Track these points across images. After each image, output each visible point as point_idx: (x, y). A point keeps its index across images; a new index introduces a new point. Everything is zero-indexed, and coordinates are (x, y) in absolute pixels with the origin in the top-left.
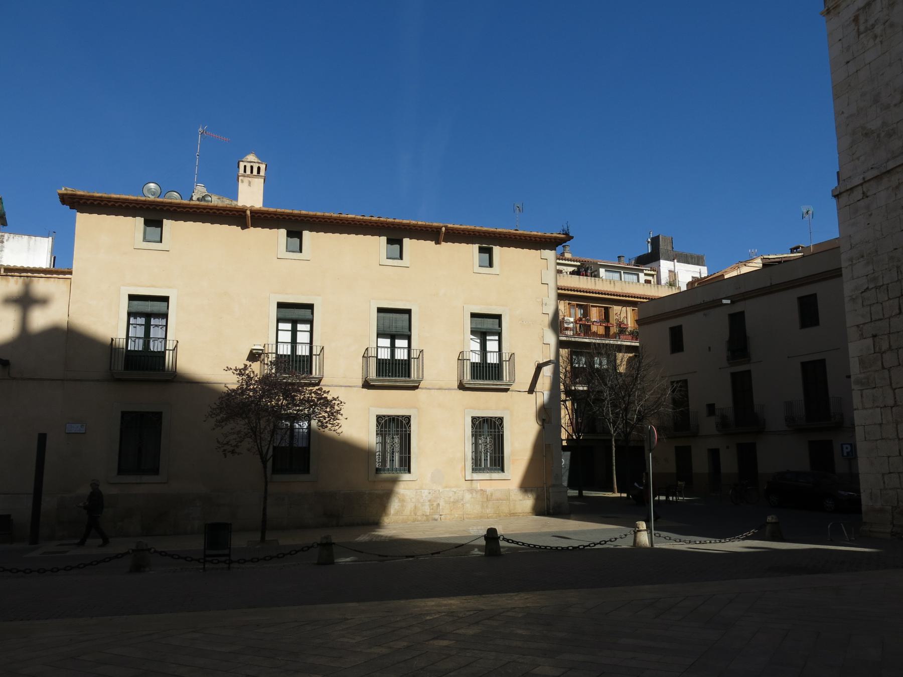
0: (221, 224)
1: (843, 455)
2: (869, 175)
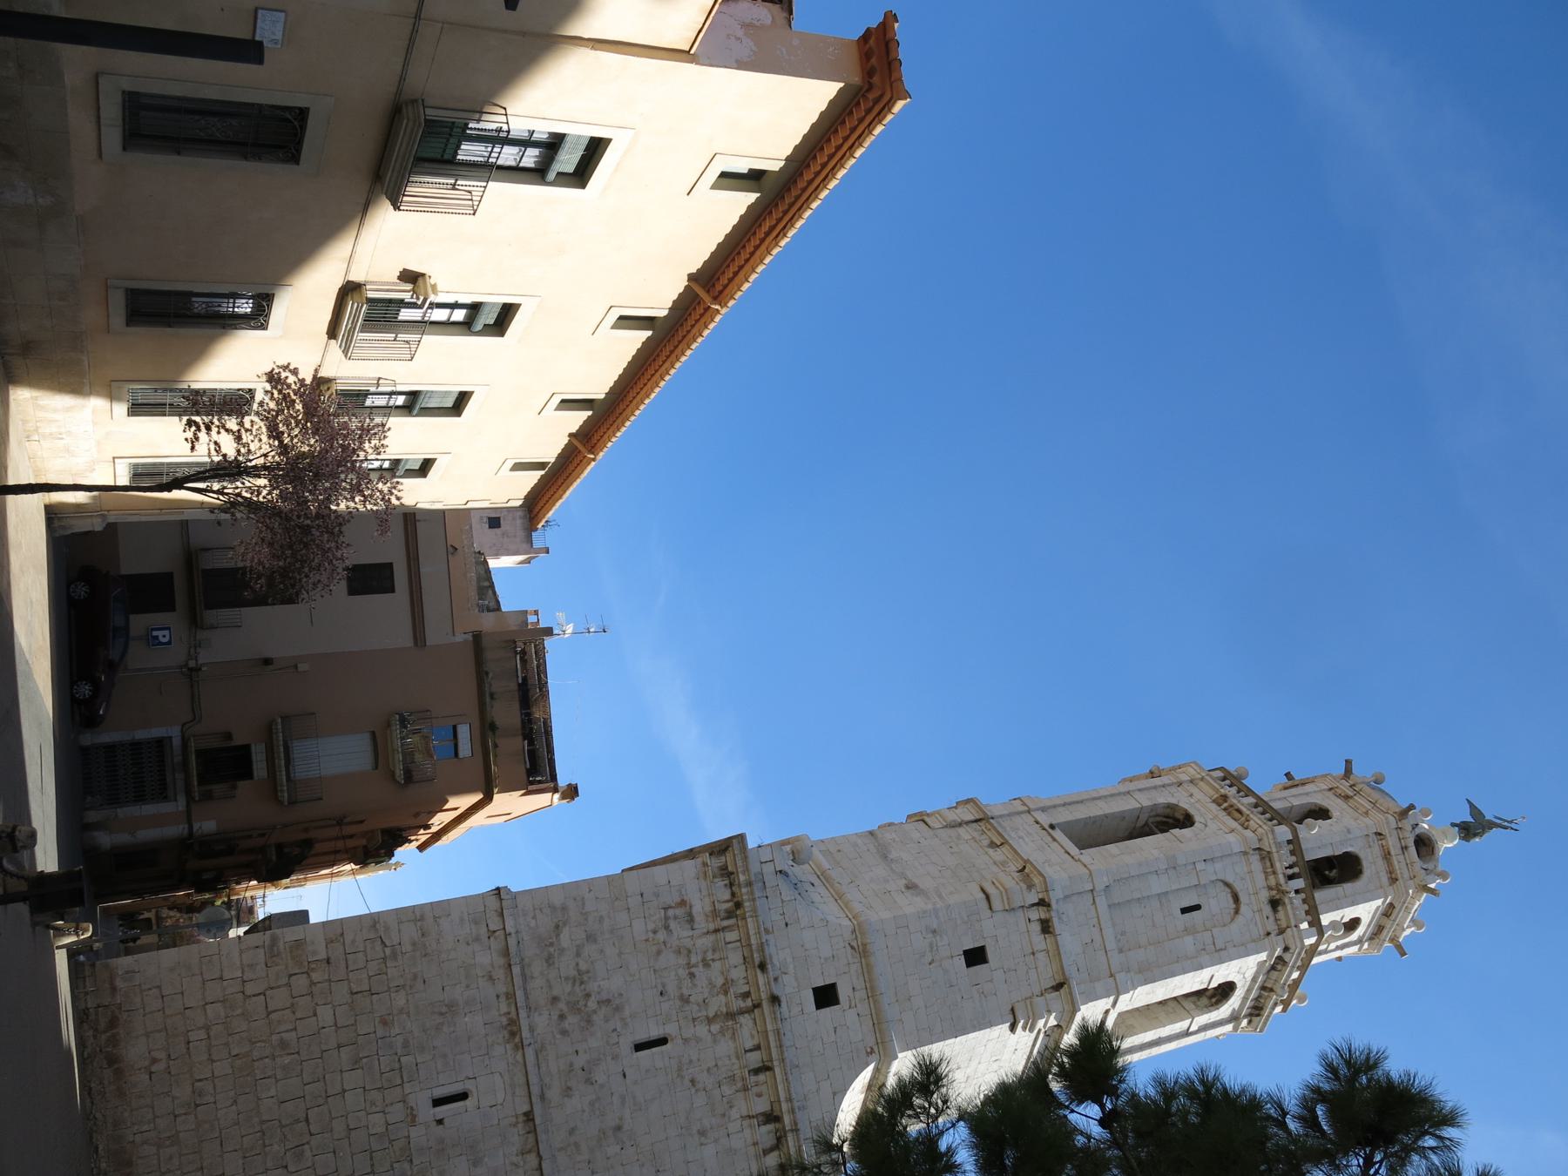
0: (712, 253)
1: (153, 630)
2: (512, 942)
